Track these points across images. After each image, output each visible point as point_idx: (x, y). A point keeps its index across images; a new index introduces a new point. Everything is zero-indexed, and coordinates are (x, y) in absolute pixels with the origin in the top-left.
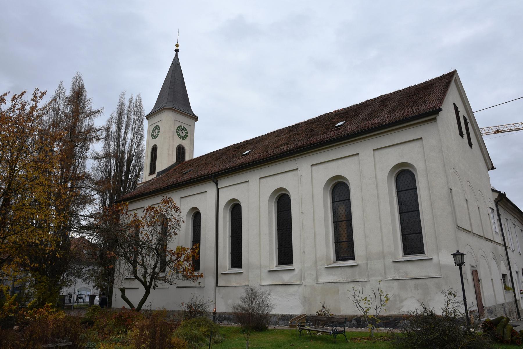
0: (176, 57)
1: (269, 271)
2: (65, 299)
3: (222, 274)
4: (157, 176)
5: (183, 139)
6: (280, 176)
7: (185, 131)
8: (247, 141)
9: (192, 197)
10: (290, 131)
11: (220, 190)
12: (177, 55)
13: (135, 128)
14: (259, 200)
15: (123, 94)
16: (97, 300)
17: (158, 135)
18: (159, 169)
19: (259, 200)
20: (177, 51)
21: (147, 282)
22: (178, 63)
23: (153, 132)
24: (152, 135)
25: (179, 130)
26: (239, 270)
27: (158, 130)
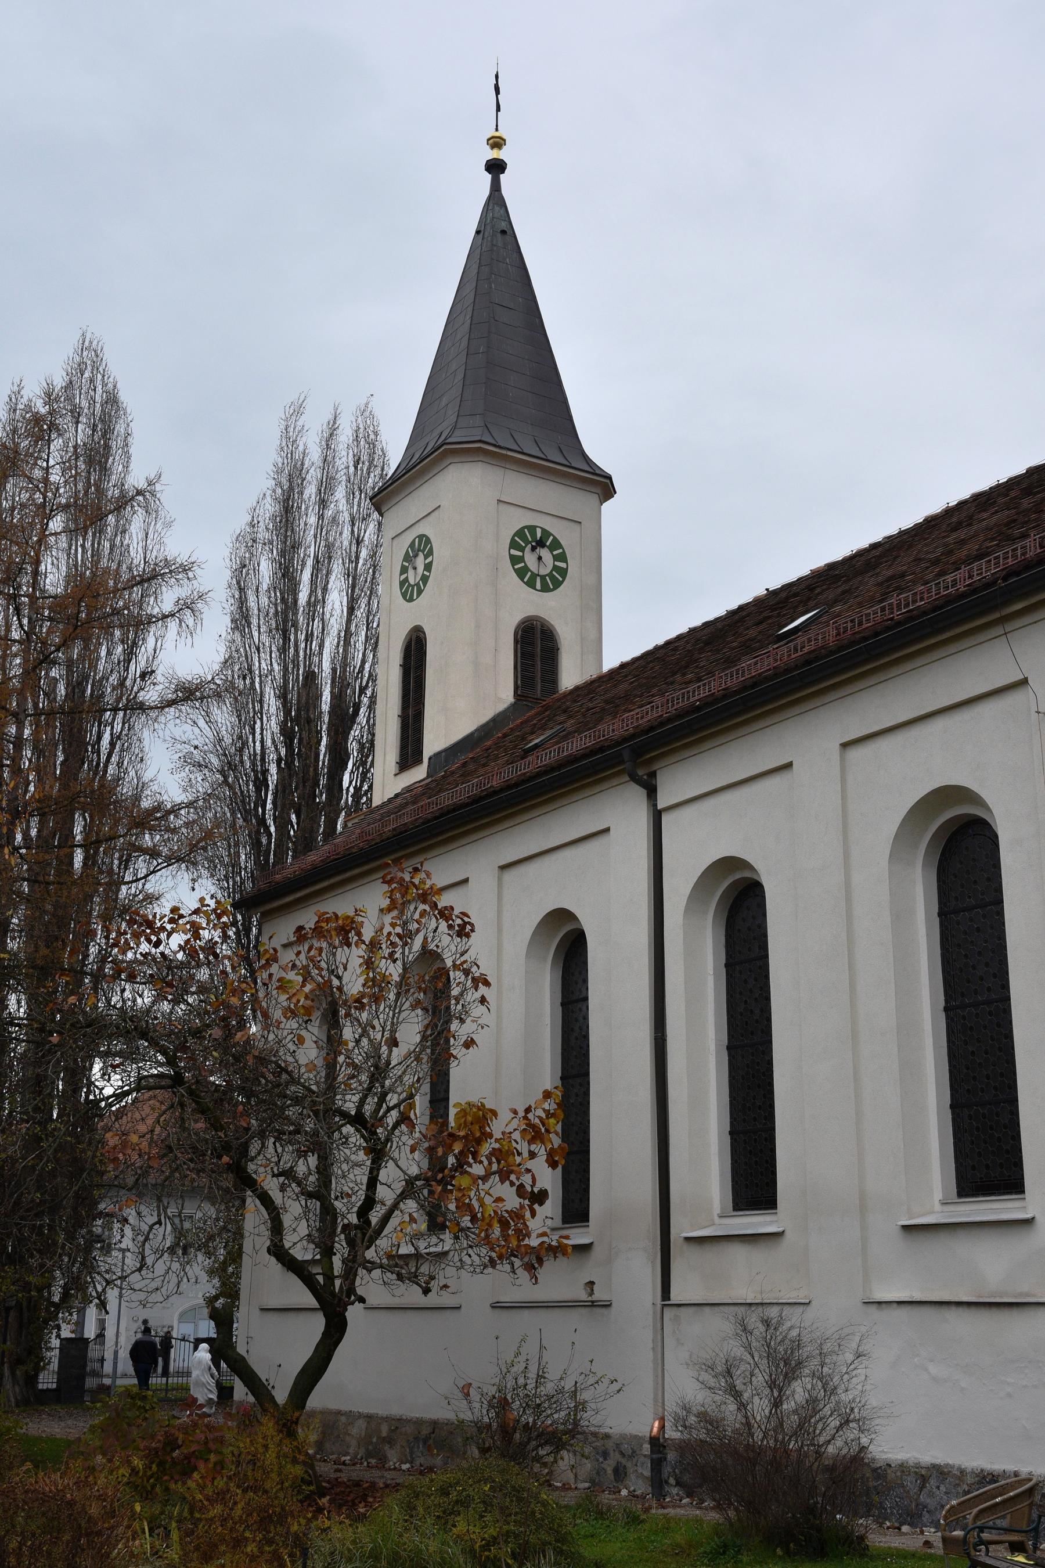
0: (496, 200)
1: (903, 1227)
2: (85, 1356)
3: (687, 1239)
4: (428, 776)
5: (545, 589)
6: (939, 724)
7: (552, 549)
8: (831, 567)
9: (547, 860)
10: (1028, 492)
11: (666, 819)
12: (496, 187)
14: (847, 856)
15: (298, 410)
16: (200, 1362)
17: (425, 579)
18: (434, 741)
19: (847, 856)
20: (496, 167)
22: (503, 225)
23: (404, 570)
24: (402, 584)
25: (522, 550)
26: (768, 1218)
27: (426, 557)
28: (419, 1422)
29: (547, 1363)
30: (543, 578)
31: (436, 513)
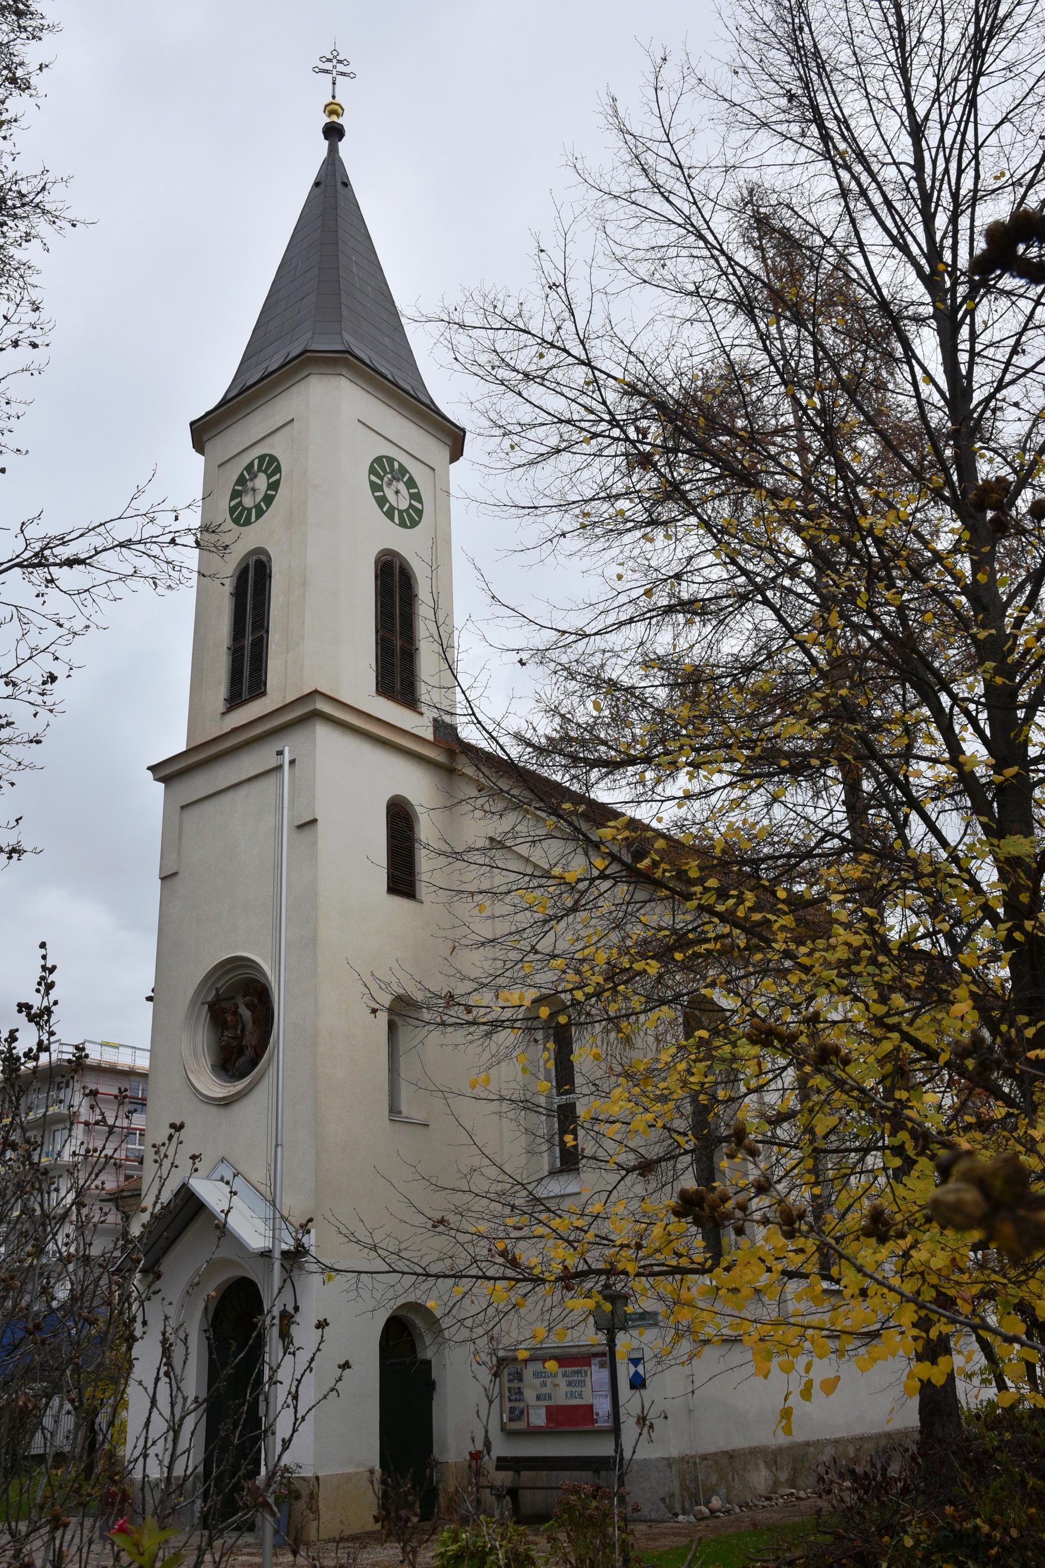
12: (333, 150)
13: (582, 949)
17: (268, 500)
21: (962, 366)
23: (235, 494)
28: (876, 1438)
29: (56, 1003)
30: (401, 512)
31: (288, 427)
